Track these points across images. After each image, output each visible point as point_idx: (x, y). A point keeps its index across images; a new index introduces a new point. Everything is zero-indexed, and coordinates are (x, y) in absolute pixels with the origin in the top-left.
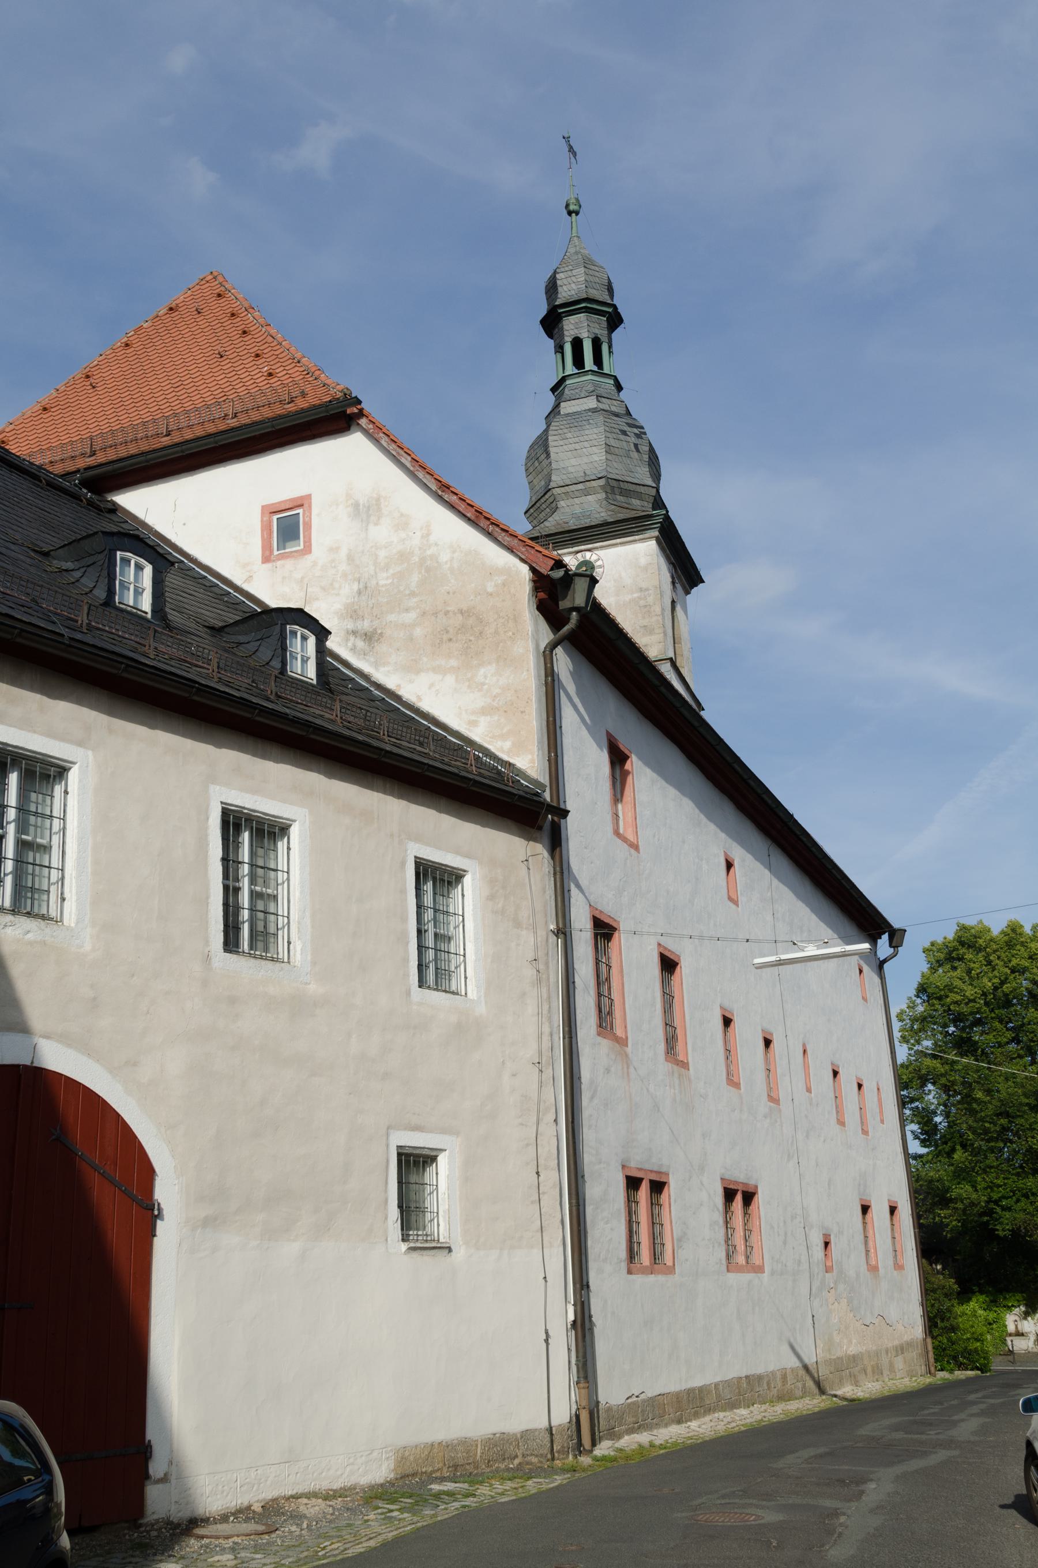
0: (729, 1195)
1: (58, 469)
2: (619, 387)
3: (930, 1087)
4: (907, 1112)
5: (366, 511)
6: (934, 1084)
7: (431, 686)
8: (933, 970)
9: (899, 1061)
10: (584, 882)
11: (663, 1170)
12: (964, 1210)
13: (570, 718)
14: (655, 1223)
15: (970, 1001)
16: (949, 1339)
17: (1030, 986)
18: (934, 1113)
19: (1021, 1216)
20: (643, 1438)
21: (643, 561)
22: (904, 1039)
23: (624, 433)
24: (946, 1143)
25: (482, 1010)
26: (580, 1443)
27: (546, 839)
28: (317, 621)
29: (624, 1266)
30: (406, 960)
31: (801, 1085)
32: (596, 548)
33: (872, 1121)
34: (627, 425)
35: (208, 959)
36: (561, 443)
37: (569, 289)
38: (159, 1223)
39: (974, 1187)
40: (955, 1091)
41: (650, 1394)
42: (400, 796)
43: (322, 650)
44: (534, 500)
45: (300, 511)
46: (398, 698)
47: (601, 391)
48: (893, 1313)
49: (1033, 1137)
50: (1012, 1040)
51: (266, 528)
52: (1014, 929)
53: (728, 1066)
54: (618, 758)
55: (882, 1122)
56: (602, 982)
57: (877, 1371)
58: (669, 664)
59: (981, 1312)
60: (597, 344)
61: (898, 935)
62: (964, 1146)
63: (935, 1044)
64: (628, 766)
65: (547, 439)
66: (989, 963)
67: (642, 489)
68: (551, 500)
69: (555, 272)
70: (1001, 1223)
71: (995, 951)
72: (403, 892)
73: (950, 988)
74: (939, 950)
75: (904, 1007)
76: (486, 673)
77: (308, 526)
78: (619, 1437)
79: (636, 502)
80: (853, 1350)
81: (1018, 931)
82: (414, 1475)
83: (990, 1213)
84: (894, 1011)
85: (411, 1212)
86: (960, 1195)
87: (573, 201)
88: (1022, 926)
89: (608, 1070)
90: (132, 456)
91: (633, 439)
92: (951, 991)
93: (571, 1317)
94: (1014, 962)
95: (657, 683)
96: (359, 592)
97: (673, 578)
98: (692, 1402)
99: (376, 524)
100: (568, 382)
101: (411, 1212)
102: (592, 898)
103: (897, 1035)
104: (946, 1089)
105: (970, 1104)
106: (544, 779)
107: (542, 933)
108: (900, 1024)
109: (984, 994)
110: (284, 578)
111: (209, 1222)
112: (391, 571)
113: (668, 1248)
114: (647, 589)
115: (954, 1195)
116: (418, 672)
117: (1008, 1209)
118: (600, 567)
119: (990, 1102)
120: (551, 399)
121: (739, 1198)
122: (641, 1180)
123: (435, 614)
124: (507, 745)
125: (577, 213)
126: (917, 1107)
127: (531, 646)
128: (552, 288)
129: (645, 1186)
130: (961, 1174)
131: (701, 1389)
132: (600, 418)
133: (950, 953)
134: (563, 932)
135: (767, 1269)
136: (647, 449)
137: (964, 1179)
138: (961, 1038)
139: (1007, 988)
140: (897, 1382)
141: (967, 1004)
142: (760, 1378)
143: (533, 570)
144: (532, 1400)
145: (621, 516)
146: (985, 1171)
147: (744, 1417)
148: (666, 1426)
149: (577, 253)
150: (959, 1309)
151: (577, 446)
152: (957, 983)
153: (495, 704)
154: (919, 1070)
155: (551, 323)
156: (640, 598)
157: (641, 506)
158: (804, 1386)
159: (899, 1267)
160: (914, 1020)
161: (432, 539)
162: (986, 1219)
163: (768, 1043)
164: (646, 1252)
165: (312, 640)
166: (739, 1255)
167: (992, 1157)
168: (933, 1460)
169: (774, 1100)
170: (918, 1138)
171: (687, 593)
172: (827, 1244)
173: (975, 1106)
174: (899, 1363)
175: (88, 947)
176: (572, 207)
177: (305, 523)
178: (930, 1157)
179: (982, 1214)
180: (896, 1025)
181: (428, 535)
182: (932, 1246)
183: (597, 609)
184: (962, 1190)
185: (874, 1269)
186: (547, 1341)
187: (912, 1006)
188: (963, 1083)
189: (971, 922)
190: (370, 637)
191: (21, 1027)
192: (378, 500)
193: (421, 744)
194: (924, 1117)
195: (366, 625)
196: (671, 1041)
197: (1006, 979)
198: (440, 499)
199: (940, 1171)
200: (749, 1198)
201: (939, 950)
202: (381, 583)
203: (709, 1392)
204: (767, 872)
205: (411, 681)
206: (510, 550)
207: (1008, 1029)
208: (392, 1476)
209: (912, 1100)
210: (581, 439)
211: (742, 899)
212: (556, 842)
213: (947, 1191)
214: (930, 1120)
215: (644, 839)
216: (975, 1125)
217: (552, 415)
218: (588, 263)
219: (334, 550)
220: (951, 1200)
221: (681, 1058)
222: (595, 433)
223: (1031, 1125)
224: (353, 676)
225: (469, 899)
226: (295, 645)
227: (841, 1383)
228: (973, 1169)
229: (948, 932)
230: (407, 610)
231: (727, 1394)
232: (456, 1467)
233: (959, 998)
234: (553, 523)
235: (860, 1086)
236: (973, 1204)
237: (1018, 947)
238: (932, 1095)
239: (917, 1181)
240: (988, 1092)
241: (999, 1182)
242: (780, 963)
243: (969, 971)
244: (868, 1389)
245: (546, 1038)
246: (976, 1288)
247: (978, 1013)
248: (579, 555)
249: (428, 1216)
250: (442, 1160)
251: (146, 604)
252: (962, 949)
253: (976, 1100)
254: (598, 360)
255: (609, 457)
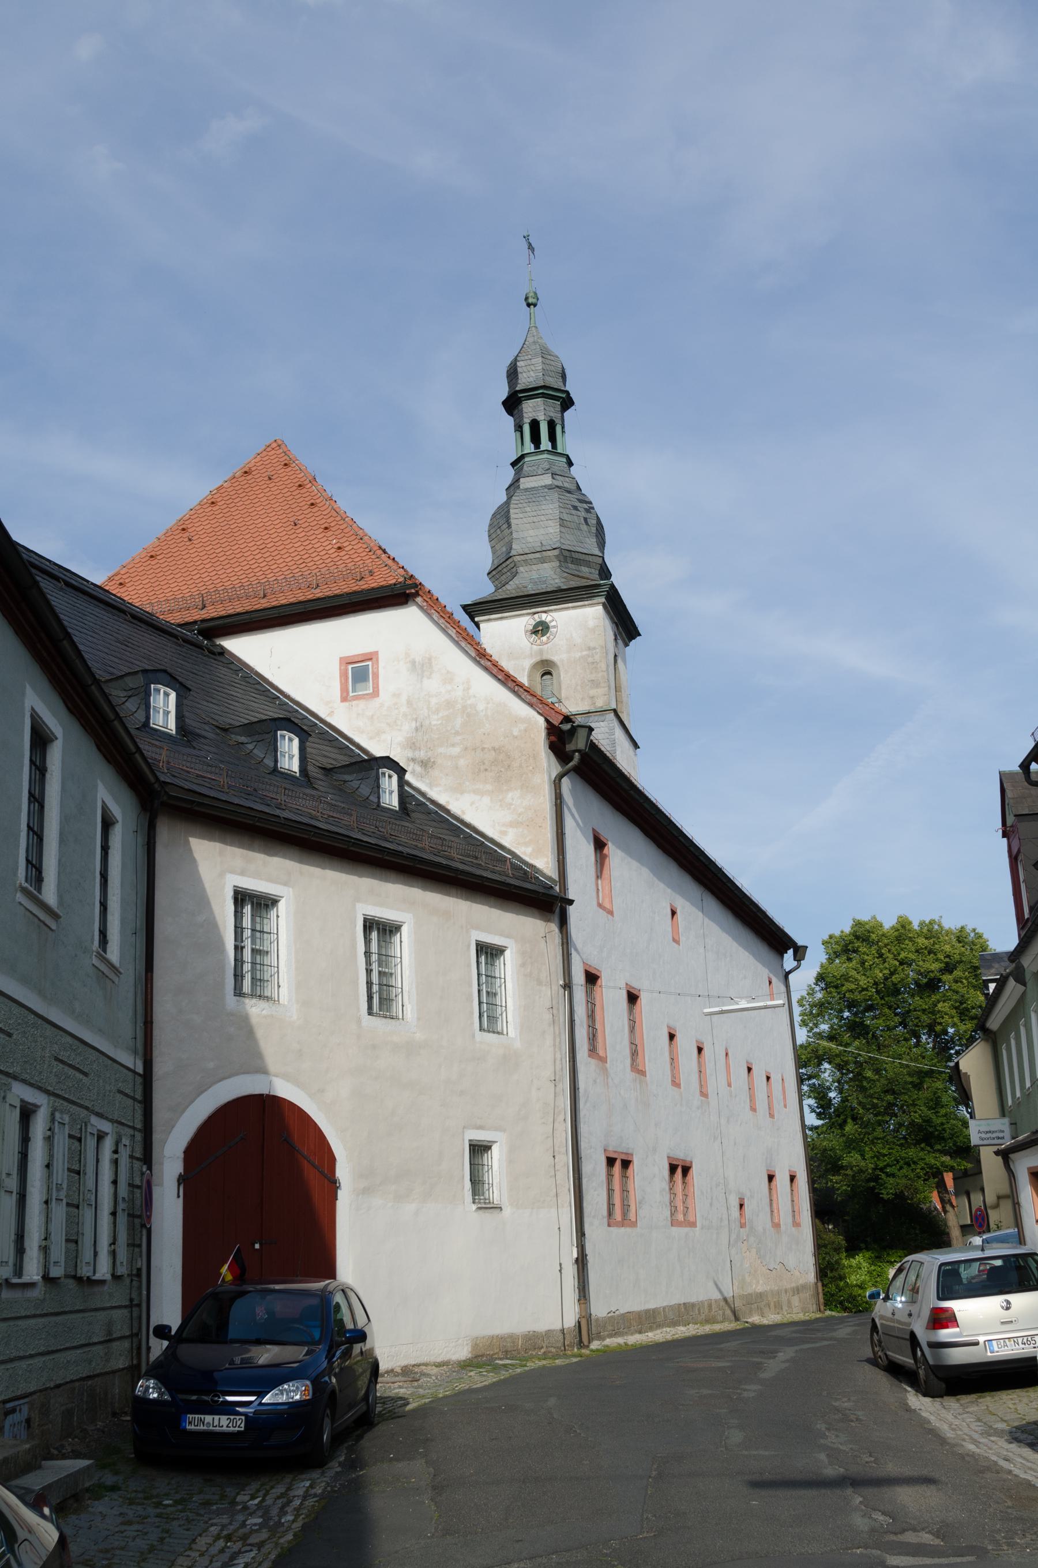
0: (673, 1168)
1: (175, 618)
2: (570, 464)
3: (826, 1065)
4: (805, 1088)
5: (421, 668)
6: (830, 1063)
7: (472, 803)
8: (831, 960)
9: (799, 1042)
10: (579, 946)
11: (630, 1151)
12: (854, 1176)
13: (570, 825)
14: (625, 1191)
15: (864, 989)
16: (837, 1286)
17: (916, 977)
18: (829, 1089)
19: (904, 1181)
20: (620, 1340)
21: (591, 624)
22: (804, 1023)
23: (575, 508)
24: (838, 1116)
25: (518, 1044)
26: (581, 1341)
27: (556, 917)
28: (398, 764)
29: (606, 1220)
30: (472, 1013)
31: (724, 1082)
32: (551, 611)
33: (777, 1105)
34: (578, 504)
35: (359, 1021)
36: (521, 516)
37: (527, 378)
38: (339, 1192)
39: (863, 1155)
40: (848, 1070)
41: (622, 1311)
42: (467, 899)
43: (402, 783)
44: (496, 563)
45: (369, 663)
46: (448, 812)
47: (555, 469)
48: (791, 1262)
49: (915, 1112)
50: (900, 1024)
51: (344, 675)
52: (903, 924)
53: (672, 1071)
54: (599, 845)
55: (785, 1106)
56: (591, 1016)
57: (778, 1306)
58: (612, 715)
59: (865, 1264)
60: (552, 425)
61: (801, 950)
62: (854, 1119)
63: (832, 1028)
64: (605, 851)
65: (508, 512)
66: (881, 955)
67: (590, 558)
68: (512, 565)
69: (515, 360)
70: (886, 1188)
71: (886, 945)
72: (469, 965)
73: (846, 978)
74: (837, 943)
75: (804, 993)
76: (513, 796)
77: (376, 676)
78: (604, 1339)
79: (585, 570)
80: (760, 1289)
81: (908, 927)
82: (482, 1356)
83: (876, 1179)
84: (795, 998)
85: (477, 1183)
86: (850, 1163)
87: (531, 294)
88: (910, 923)
89: (595, 1081)
90: (239, 614)
91: (583, 514)
92: (847, 980)
93: (575, 1255)
94: (903, 955)
95: (627, 788)
96: (417, 729)
97: (615, 636)
98: (648, 1319)
99: (429, 678)
100: (526, 459)
101: (477, 1183)
102: (584, 957)
103: (797, 1019)
104: (839, 1067)
105: (861, 1081)
106: (555, 876)
107: (555, 988)
108: (801, 1009)
109: (876, 983)
110: (358, 714)
111: (366, 1191)
112: (441, 715)
113: (633, 1208)
114: (594, 648)
115: (845, 1163)
116: (462, 793)
117: (893, 1175)
118: (554, 627)
119: (878, 1080)
120: (511, 472)
121: (679, 1171)
122: (615, 1159)
123: (475, 749)
124: (529, 850)
125: (535, 305)
126: (814, 1084)
127: (546, 778)
128: (513, 373)
129: (619, 1163)
130: (851, 1144)
131: (654, 1310)
132: (555, 495)
133: (846, 945)
134: (568, 986)
135: (698, 1224)
136: (595, 522)
137: (854, 1149)
138: (855, 1022)
139: (895, 978)
140: (794, 1316)
141: (860, 992)
142: (693, 1305)
143: (547, 721)
144: (551, 1311)
145: (573, 584)
146: (872, 1142)
147: (682, 1331)
148: (632, 1334)
149: (534, 342)
150: (846, 1262)
151: (535, 519)
152: (853, 973)
153: (520, 820)
154: (817, 1051)
155: (512, 404)
156: (588, 656)
157: (591, 574)
158: (724, 1314)
159: (796, 1224)
160: (812, 1006)
161: (471, 692)
162: (872, 1184)
163: (700, 1050)
164: (620, 1213)
165: (395, 778)
166: (680, 1215)
167: (879, 1129)
168: (818, 1345)
169: (704, 1094)
170: (815, 1111)
171: (626, 645)
172: (741, 1206)
173: (865, 1084)
174: (796, 1301)
175: (295, 1017)
176: (531, 300)
177: (373, 673)
178: (824, 1129)
179: (868, 1180)
180: (797, 1010)
181: (468, 689)
182: (823, 1209)
183: (593, 747)
184: (853, 1159)
185: (777, 1226)
186: (560, 1271)
187: (811, 993)
188: (856, 1063)
189: (865, 917)
190: (425, 764)
191: (263, 1071)
192: (430, 659)
193: (477, 858)
194: (820, 1094)
195: (422, 754)
196: (634, 1054)
197: (896, 970)
198: (478, 663)
199: (833, 1142)
200: (686, 1170)
201: (837, 943)
202: (434, 723)
203: (659, 1313)
204: (700, 914)
205: (457, 800)
206: (531, 705)
207: (896, 1014)
208: (470, 1355)
209: (810, 1078)
210: (539, 513)
211: (682, 939)
212: (563, 922)
213: (839, 1159)
214: (825, 1096)
215: (617, 905)
216: (864, 1101)
217: (512, 488)
218: (545, 353)
219: (397, 695)
220: (842, 1167)
221: (640, 1068)
222: (551, 508)
223: (913, 1101)
224: (413, 793)
225: (508, 966)
226: (385, 782)
227: (751, 1315)
228: (862, 1139)
229: (844, 927)
230: (453, 745)
231: (671, 1315)
232: (506, 1352)
233: (853, 986)
234: (514, 586)
235: (768, 1078)
236: (861, 1171)
237: (907, 942)
238: (827, 1072)
239: (812, 1149)
240: (877, 1071)
241: (885, 1151)
242: (722, 1012)
243: (863, 963)
244: (771, 1318)
245: (558, 1062)
246: (863, 1245)
247: (870, 1000)
248: (536, 616)
249: (486, 1186)
250: (495, 1148)
251: (295, 767)
252: (856, 943)
253: (866, 1078)
254: (552, 438)
255: (563, 529)
